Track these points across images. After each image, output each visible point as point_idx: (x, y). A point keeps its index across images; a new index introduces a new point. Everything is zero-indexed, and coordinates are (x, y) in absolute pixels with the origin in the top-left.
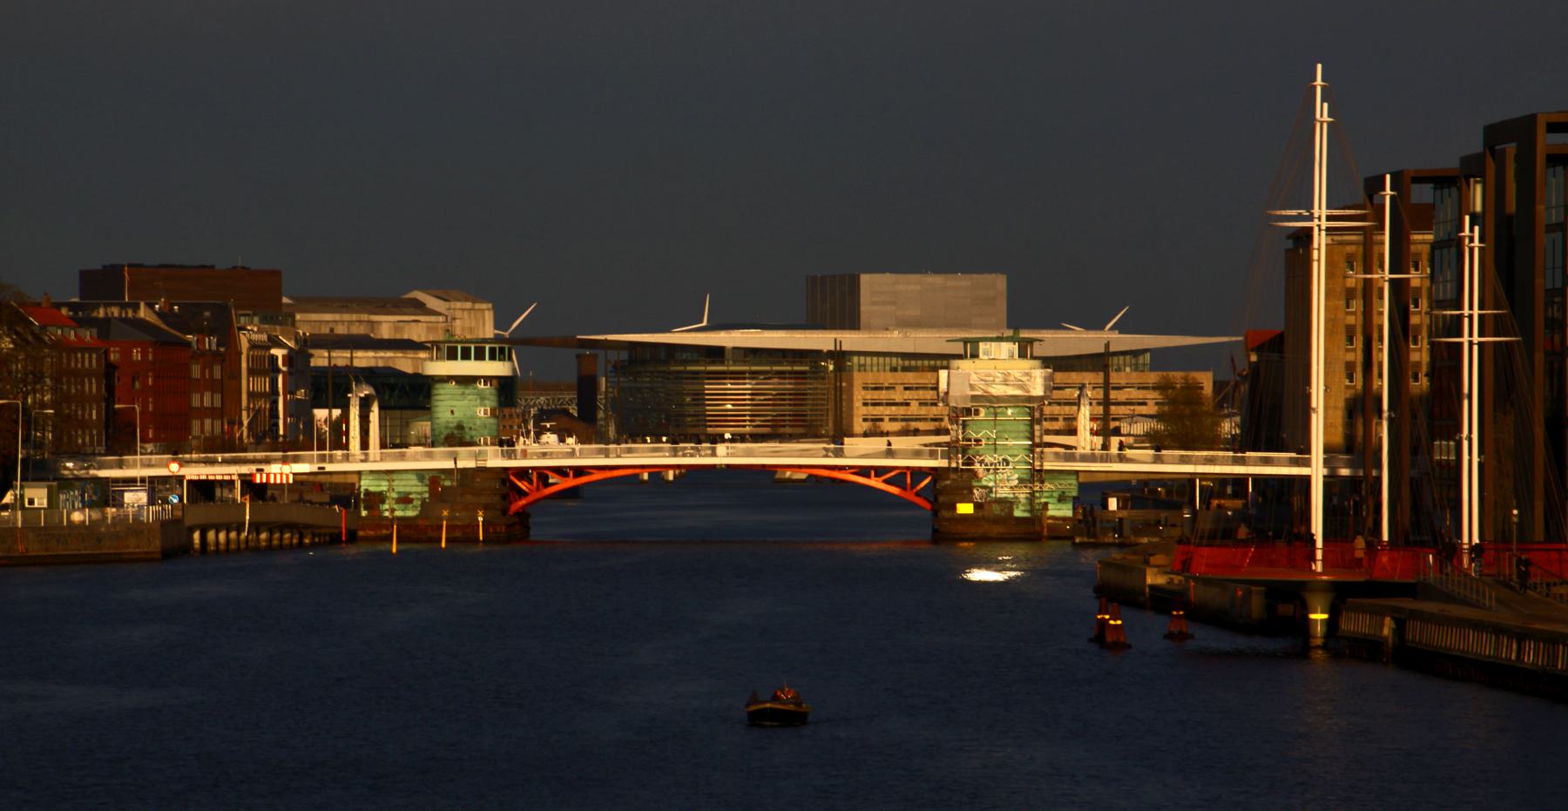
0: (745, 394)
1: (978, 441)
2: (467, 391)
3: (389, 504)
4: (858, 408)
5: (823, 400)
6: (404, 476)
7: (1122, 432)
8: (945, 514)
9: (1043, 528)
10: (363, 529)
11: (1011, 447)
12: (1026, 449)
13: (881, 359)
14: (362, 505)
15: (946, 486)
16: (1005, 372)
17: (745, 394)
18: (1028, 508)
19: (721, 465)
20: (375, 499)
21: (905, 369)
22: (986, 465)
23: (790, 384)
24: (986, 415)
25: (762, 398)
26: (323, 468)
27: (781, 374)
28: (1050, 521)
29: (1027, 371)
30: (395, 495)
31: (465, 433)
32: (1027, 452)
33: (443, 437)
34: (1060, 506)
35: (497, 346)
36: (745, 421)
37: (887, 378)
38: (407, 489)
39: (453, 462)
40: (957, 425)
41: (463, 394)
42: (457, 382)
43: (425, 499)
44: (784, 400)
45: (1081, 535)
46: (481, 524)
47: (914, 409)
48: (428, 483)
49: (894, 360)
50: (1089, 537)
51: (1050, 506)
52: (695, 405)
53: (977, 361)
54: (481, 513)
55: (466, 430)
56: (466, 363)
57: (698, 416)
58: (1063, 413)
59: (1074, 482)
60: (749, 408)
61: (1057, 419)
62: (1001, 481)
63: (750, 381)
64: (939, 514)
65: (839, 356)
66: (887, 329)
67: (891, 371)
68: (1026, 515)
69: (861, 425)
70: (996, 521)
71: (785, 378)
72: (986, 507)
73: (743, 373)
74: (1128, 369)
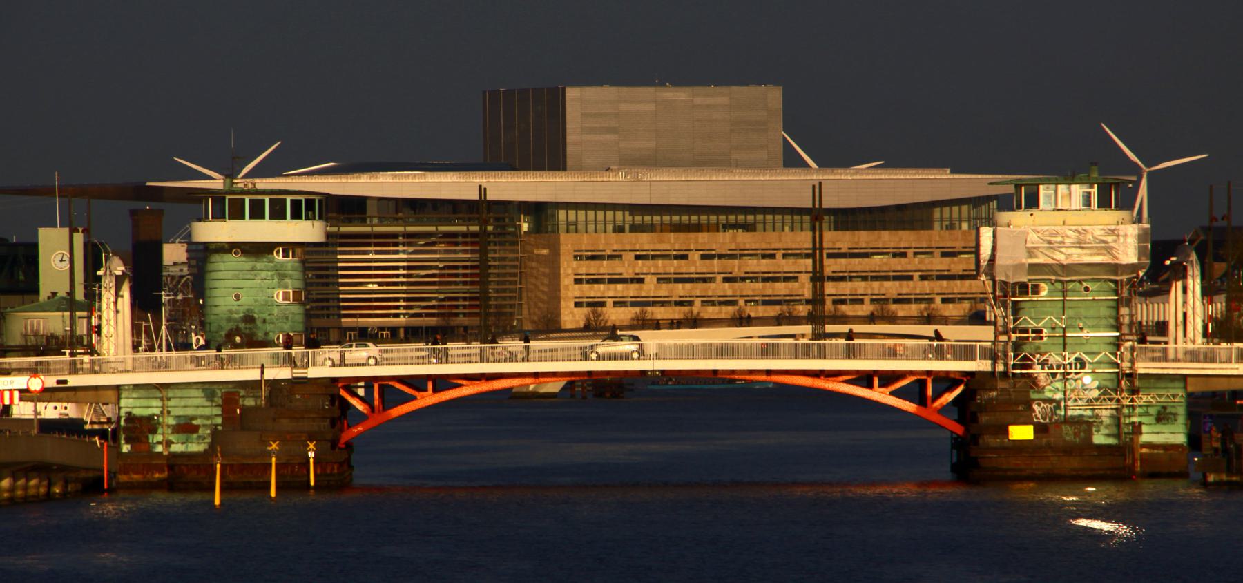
0: (397, 268)
1: (1038, 331)
2: (259, 266)
3: (163, 434)
4: (567, 287)
5: (515, 275)
6: (187, 392)
7: (988, 319)
8: (992, 441)
9: (1134, 460)
10: (126, 473)
11: (1088, 340)
12: (1110, 344)
13: (600, 214)
14: (123, 436)
15: (992, 399)
16: (1080, 229)
17: (397, 268)
18: (1114, 430)
19: (654, 371)
20: (140, 427)
21: (635, 229)
22: (1051, 367)
23: (465, 252)
24: (1050, 292)
25: (423, 273)
26: (65, 382)
27: (450, 238)
28: (1144, 450)
29: (1113, 227)
30: (172, 421)
31: (256, 327)
32: (1112, 348)
33: (223, 333)
34: (1159, 428)
35: (302, 198)
36: (397, 307)
37: (609, 242)
38: (190, 412)
39: (259, 371)
40: (1005, 307)
41: (253, 269)
42: (243, 252)
43: (217, 425)
44: (456, 275)
45: (1216, 471)
46: (311, 460)
47: (650, 288)
48: (220, 402)
49: (619, 214)
50: (1229, 472)
51: (1144, 429)
52: (318, 284)
53: (1036, 213)
54: (311, 446)
55: (259, 323)
56: (257, 223)
57: (327, 300)
58: (869, 292)
59: (1181, 392)
60: (405, 288)
61: (861, 302)
62: (1072, 390)
63: (405, 248)
64: (981, 441)
65: (539, 211)
66: (608, 170)
67: (614, 231)
68: (1111, 441)
69: (572, 313)
70: (1068, 450)
71: (456, 244)
72: (1052, 430)
73: (395, 235)
74: (965, 226)
